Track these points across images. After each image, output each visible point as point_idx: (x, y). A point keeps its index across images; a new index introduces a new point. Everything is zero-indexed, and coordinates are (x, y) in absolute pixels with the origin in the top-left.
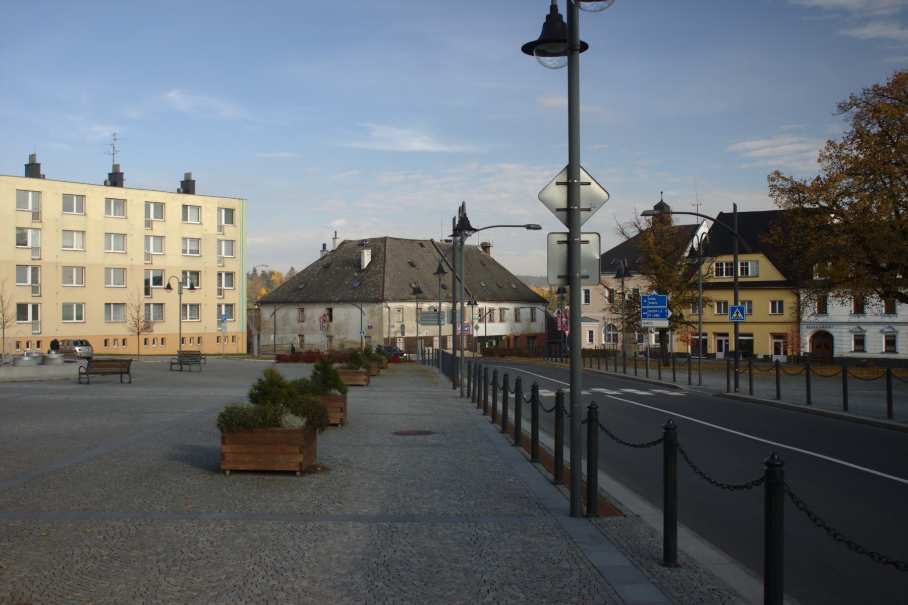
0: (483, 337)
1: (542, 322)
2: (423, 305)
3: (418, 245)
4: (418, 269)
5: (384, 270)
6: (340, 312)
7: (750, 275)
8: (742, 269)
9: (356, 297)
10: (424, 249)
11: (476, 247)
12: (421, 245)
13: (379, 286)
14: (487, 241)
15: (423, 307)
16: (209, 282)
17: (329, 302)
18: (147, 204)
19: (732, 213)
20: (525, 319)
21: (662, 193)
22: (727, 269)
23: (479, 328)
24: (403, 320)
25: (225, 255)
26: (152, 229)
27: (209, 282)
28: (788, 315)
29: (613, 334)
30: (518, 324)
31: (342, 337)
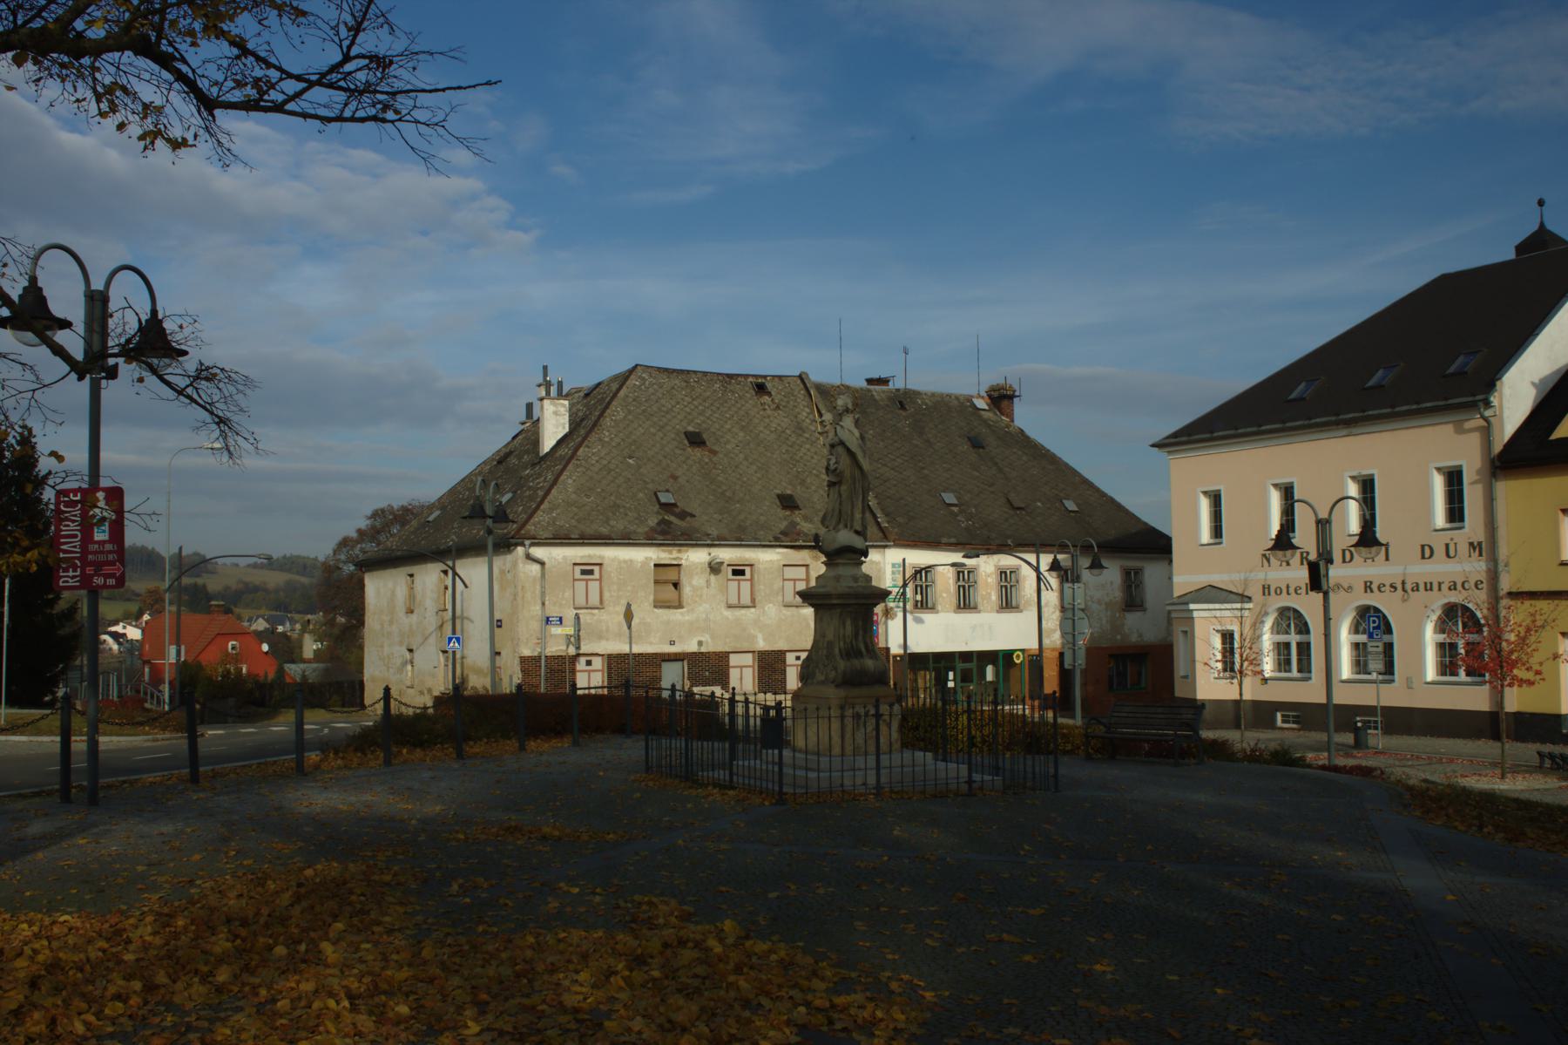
0: (785, 662)
4: (714, 453)
10: (766, 399)
11: (969, 399)
12: (761, 388)
14: (1002, 381)
15: (683, 562)
20: (1099, 602)
21: (1541, 203)
24: (753, 600)
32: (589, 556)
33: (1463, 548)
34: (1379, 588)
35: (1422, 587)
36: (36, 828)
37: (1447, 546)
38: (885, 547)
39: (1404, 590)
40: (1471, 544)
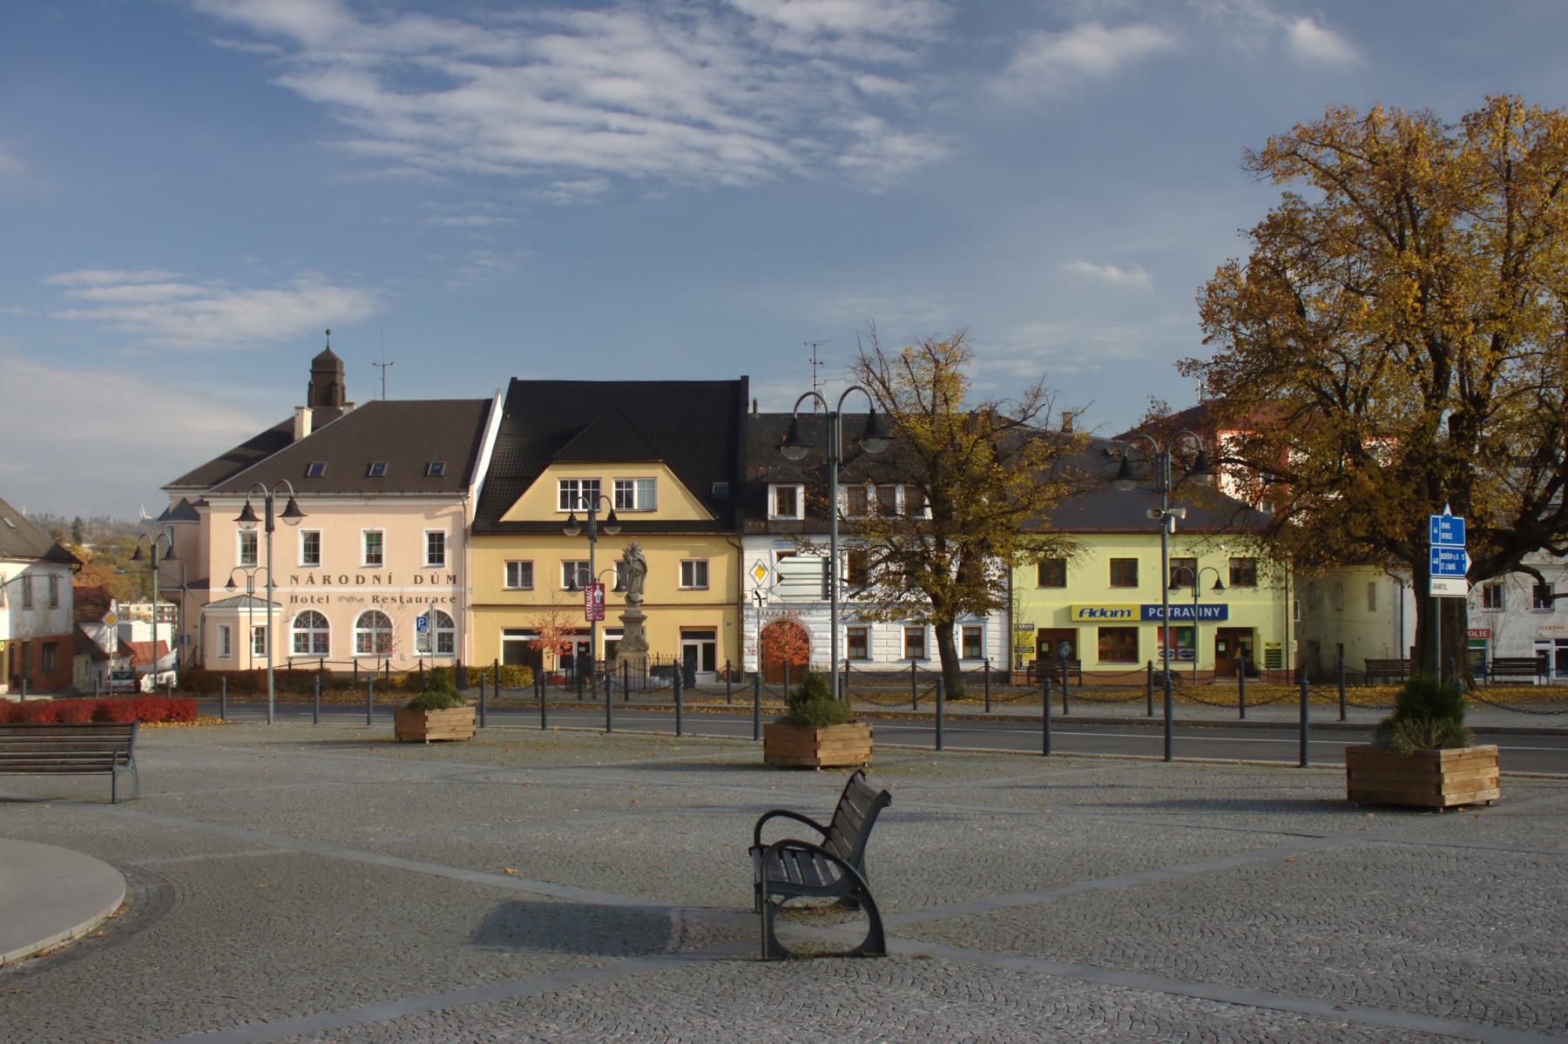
7: (636, 506)
22: (585, 494)
28: (718, 587)
29: (315, 634)
30: (28, 614)
33: (443, 579)
35: (414, 600)
36: (762, 622)
37: (432, 577)
40: (449, 576)
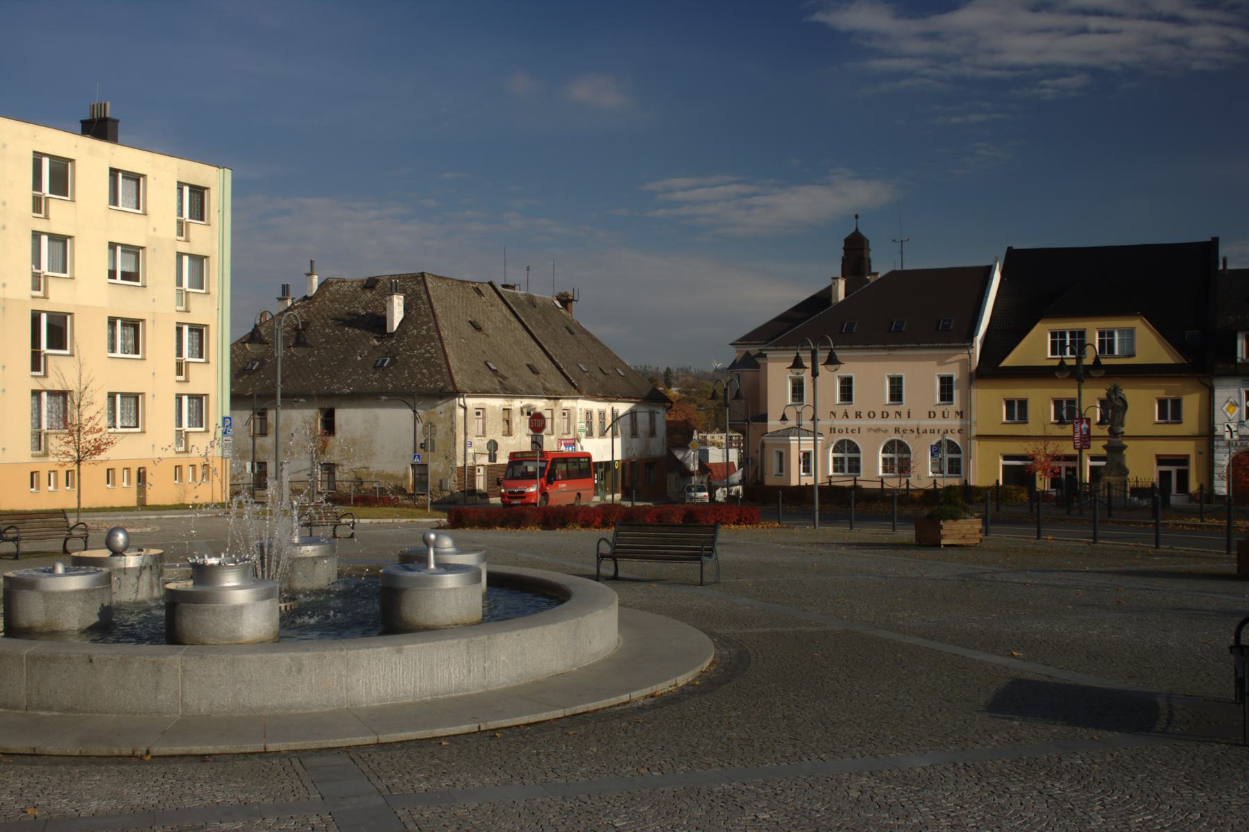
1: (663, 438)
2: (512, 403)
3: (473, 291)
5: (439, 335)
6: (349, 418)
7: (1116, 352)
8: (1053, 344)
9: (390, 386)
13: (440, 365)
15: (512, 407)
16: (160, 342)
17: (331, 396)
18: (37, 158)
19: (1209, 242)
23: (511, 453)
25: (190, 287)
26: (47, 217)
27: (160, 342)
29: (849, 458)
31: (359, 465)
32: (481, 404)
33: (952, 414)
34: (904, 431)
35: (928, 431)
37: (943, 412)
38: (577, 398)
39: (918, 432)
40: (957, 412)
